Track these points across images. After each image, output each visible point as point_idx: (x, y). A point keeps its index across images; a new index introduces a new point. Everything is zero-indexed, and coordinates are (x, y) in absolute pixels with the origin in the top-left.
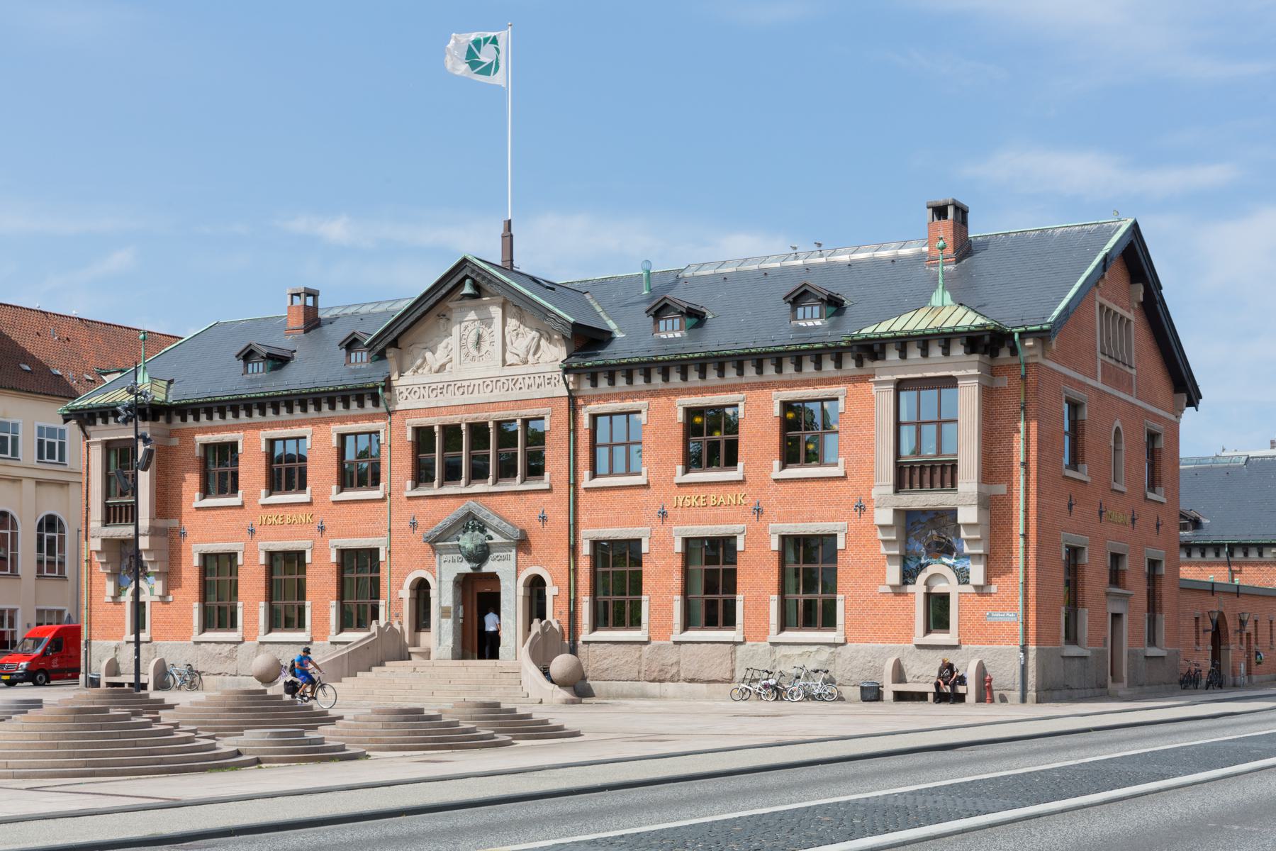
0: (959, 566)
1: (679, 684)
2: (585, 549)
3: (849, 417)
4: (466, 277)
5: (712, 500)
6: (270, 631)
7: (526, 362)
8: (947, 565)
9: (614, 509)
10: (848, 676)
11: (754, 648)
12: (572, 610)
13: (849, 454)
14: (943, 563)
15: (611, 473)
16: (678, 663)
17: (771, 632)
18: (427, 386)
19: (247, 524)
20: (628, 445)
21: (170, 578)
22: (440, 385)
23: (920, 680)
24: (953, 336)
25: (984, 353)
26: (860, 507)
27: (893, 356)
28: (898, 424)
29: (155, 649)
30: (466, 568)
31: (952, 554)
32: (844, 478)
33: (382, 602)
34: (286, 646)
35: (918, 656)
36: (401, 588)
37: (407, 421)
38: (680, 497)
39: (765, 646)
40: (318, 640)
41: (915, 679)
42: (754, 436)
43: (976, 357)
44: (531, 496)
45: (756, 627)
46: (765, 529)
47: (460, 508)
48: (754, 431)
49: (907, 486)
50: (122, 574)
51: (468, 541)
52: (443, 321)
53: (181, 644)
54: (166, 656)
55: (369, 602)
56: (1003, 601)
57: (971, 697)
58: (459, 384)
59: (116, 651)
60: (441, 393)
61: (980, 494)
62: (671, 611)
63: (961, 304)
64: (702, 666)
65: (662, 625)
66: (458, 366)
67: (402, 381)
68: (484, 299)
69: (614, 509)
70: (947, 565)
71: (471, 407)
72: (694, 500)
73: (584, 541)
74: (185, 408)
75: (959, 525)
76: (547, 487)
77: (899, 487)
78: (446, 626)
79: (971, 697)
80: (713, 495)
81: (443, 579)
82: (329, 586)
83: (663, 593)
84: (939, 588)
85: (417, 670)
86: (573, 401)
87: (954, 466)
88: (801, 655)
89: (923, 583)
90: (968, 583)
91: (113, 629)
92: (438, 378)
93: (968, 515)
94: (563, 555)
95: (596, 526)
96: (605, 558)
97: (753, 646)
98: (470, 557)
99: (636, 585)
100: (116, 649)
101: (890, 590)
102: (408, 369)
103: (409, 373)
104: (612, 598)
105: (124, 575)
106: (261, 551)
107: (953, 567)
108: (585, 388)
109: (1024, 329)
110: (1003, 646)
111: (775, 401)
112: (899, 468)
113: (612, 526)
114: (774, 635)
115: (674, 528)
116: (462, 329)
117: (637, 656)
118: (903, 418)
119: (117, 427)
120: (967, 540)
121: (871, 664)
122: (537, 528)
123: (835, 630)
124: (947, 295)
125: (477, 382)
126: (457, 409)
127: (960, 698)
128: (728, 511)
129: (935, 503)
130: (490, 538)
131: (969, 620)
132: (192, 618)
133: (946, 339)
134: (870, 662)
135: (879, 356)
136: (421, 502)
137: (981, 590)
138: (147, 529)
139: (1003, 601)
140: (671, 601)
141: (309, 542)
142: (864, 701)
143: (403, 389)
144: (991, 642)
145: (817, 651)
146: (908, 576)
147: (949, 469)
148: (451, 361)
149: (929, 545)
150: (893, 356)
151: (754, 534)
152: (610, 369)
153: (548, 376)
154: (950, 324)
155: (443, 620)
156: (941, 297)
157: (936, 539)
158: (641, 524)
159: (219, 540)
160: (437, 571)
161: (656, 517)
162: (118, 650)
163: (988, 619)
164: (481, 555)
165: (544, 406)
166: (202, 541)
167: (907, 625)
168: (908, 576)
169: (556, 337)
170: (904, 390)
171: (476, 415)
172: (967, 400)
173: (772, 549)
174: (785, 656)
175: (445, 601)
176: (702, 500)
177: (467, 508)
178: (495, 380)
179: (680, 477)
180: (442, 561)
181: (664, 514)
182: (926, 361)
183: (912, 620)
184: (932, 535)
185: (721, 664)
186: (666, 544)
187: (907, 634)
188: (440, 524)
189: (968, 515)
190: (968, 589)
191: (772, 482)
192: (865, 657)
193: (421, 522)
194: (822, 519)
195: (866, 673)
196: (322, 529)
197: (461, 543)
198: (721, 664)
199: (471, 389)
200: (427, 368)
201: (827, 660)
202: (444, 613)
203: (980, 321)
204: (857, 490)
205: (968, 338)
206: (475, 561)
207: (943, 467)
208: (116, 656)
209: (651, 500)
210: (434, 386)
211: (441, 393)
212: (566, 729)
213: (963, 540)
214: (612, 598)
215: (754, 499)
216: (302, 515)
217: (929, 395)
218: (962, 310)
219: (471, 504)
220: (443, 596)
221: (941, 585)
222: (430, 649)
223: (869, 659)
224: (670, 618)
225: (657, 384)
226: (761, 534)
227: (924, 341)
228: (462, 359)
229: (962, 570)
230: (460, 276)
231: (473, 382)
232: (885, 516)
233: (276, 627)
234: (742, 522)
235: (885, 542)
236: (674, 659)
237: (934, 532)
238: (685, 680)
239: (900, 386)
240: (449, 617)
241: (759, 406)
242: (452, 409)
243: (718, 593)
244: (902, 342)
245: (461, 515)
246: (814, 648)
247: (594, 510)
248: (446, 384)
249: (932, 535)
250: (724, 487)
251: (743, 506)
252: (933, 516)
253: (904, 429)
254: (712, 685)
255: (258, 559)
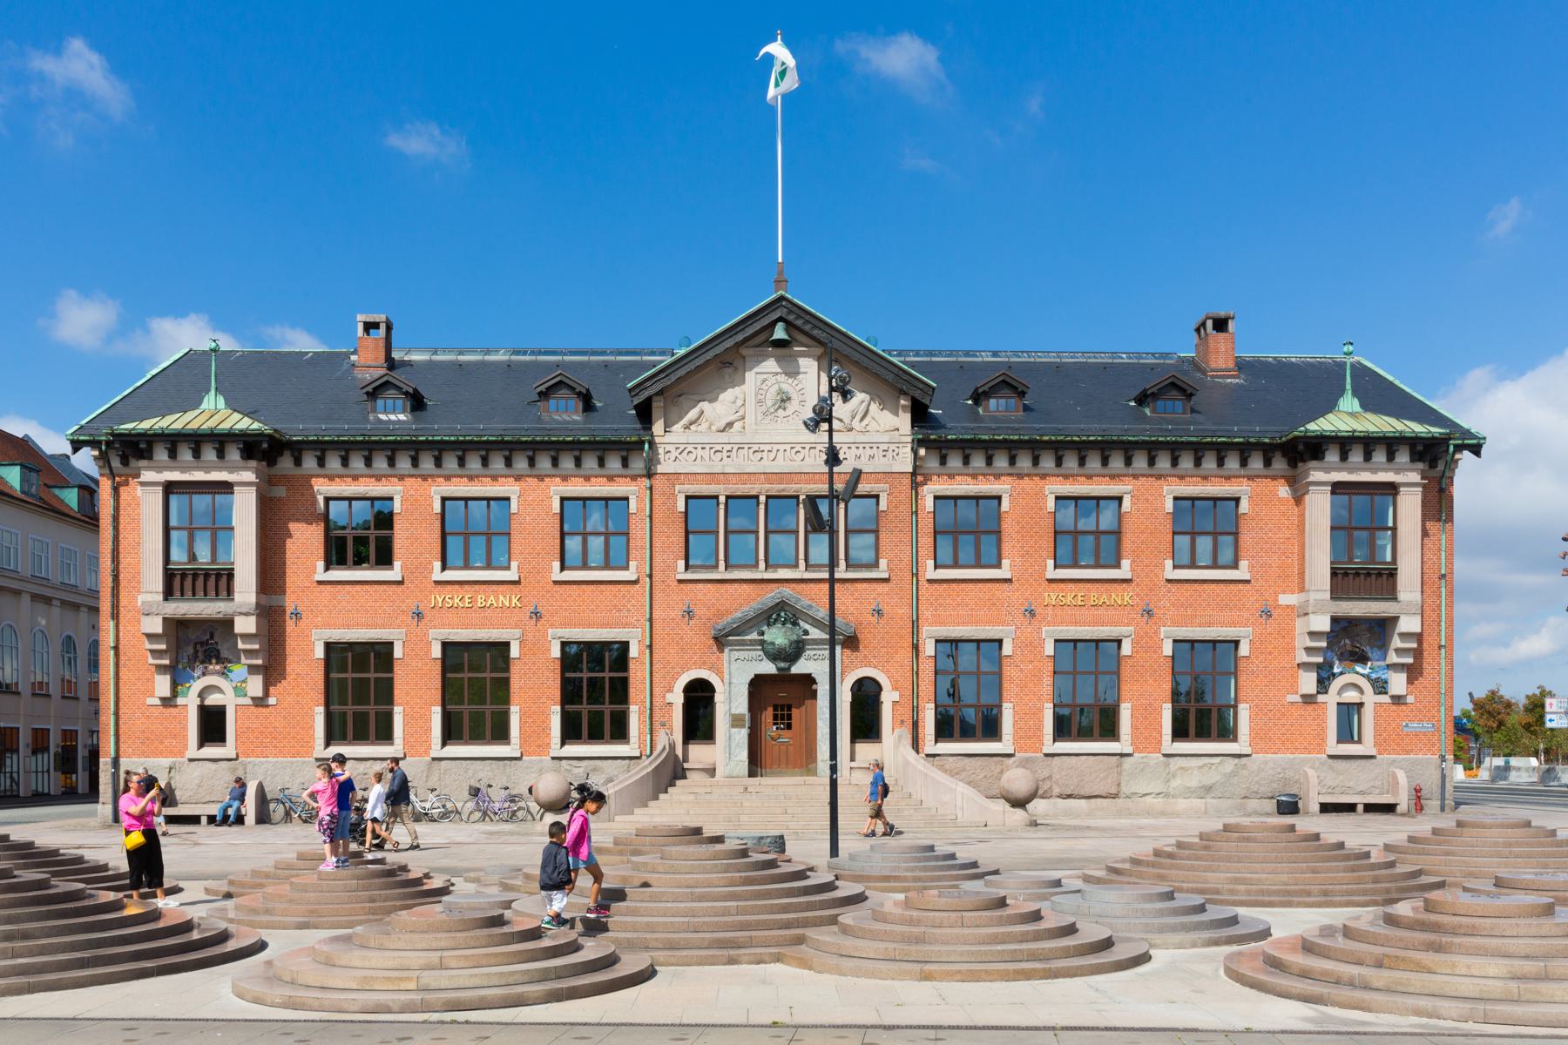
0: (1374, 676)
1: (1052, 800)
2: (929, 648)
3: (1253, 519)
4: (780, 319)
5: (480, 601)
6: (444, 744)
7: (851, 430)
8: (1362, 675)
9: (967, 605)
10: (1255, 788)
11: (1145, 760)
12: (1356, 717)
13: (1253, 557)
14: (1357, 673)
15: (585, 566)
16: (1050, 777)
17: (1164, 743)
18: (708, 447)
19: (411, 604)
20: (489, 535)
21: (272, 669)
22: (728, 447)
23: (1336, 791)
24: (180, 439)
25: (260, 460)
26: (296, 615)
27: (161, 454)
28: (167, 530)
29: (245, 769)
30: (769, 668)
31: (1366, 664)
32: (401, 583)
33: (634, 710)
34: (478, 762)
35: (1331, 767)
36: (670, 690)
37: (677, 487)
38: (1052, 596)
39: (1157, 758)
40: (530, 755)
41: (1330, 790)
42: (1142, 532)
43: (253, 463)
44: (859, 586)
45: (1146, 738)
46: (1156, 633)
47: (770, 596)
48: (1143, 527)
49: (178, 593)
50: (180, 666)
51: (778, 636)
52: (728, 370)
53: (292, 763)
54: (265, 779)
55: (607, 708)
56: (1420, 711)
57: (250, 818)
58: (755, 447)
59: (170, 772)
60: (728, 457)
61: (258, 604)
62: (1041, 720)
63: (235, 411)
64: (1082, 780)
65: (1028, 735)
66: (754, 427)
67: (668, 438)
68: (796, 349)
69: (967, 605)
70: (1362, 675)
71: (774, 477)
72: (457, 600)
73: (927, 640)
74: (300, 446)
75: (236, 636)
76: (634, 578)
77: (168, 593)
78: (738, 737)
79: (250, 818)
80: (1095, 594)
81: (734, 680)
82: (548, 687)
83: (1030, 700)
84: (213, 700)
85: (750, 789)
86: (917, 477)
87: (230, 575)
88: (1200, 767)
89: (197, 694)
90: (1386, 693)
91: (162, 742)
92: (724, 437)
93: (245, 625)
94: (905, 655)
95: (943, 624)
96: (344, 661)
97: (1143, 758)
98: (775, 655)
99: (386, 693)
100: (171, 769)
101: (1300, 700)
102: (676, 422)
103: (678, 427)
104: (350, 708)
105: (185, 668)
106: (434, 642)
107: (1368, 677)
108: (1047, 465)
109: (1460, 442)
110: (1420, 756)
111: (1168, 496)
112: (169, 576)
113: (964, 624)
114: (436, 750)
115: (1044, 629)
116: (759, 382)
117: (999, 770)
118: (173, 522)
119: (195, 465)
120: (245, 651)
121: (1281, 775)
122: (869, 623)
123: (392, 744)
124: (1356, 402)
125: (782, 447)
126: (752, 478)
127: (240, 820)
128: (1111, 612)
129: (1378, 611)
130: (806, 633)
131: (1385, 730)
132: (312, 727)
133: (221, 441)
134: (1279, 773)
135: (145, 454)
136: (700, 586)
137: (259, 702)
138: (254, 606)
139: (1420, 711)
140: (1041, 710)
141: (517, 632)
142: (1280, 814)
143: (671, 448)
144: (1408, 753)
145: (1220, 763)
146: (1323, 684)
147: (225, 578)
148: (743, 418)
149: (1342, 654)
150: (1332, 456)
151: (1142, 638)
152: (148, 439)
153: (884, 447)
154: (226, 426)
155: (733, 730)
156: (1349, 403)
157: (1349, 648)
158: (1003, 623)
159: (358, 625)
160: (726, 671)
161: (1021, 616)
162: (173, 771)
163: (1405, 729)
164: (795, 651)
165: (878, 481)
166: (329, 626)
167: (1318, 735)
168: (1323, 684)
169: (902, 402)
170: (173, 493)
171: (782, 486)
172: (244, 510)
173: (1164, 654)
174: (1182, 768)
175: (737, 707)
176: (1080, 599)
177: (779, 596)
178: (808, 446)
179: (321, 575)
180: (733, 659)
181: (1032, 613)
182: (1367, 465)
183: (1324, 730)
184: (1345, 644)
185: (1106, 777)
186: (1035, 645)
187: (1319, 745)
188: (739, 615)
189: (245, 625)
190: (1385, 699)
191: (315, 584)
192: (1273, 769)
193: (699, 611)
194: (1223, 624)
195: (1275, 785)
196: (536, 615)
197: (766, 637)
198: (1106, 777)
199: (772, 455)
200: (704, 426)
201: (1232, 772)
202: (736, 721)
203: (256, 426)
204: (1262, 595)
205: (245, 443)
206: (784, 660)
207: (184, 576)
208: (170, 778)
209: (1013, 597)
210: (718, 447)
211: (728, 457)
212: (87, 862)
213: (240, 650)
214: (350, 708)
215: (1142, 600)
216: (1117, 595)
217: (201, 502)
218: (237, 416)
219: (787, 591)
220: (731, 701)
221: (212, 697)
222: (715, 764)
223: (1279, 770)
224: (1040, 728)
225: (1023, 468)
226: (1151, 638)
227: (197, 441)
228: (759, 418)
229: (1377, 680)
230: (774, 316)
231: (776, 447)
232: (1323, 624)
233: (450, 739)
234: (1128, 625)
235: (152, 651)
236: (1046, 773)
237: (1347, 641)
238: (1060, 796)
239: (170, 488)
240: (743, 726)
241: (1147, 500)
242: (746, 477)
243: (369, 704)
244: (173, 441)
245: (770, 604)
246: (1217, 760)
247: (940, 605)
248: (736, 447)
249: (1345, 644)
250: (1107, 585)
251: (1129, 608)
252: (1346, 625)
253: (174, 535)
254: (1093, 800)
255: (429, 651)
